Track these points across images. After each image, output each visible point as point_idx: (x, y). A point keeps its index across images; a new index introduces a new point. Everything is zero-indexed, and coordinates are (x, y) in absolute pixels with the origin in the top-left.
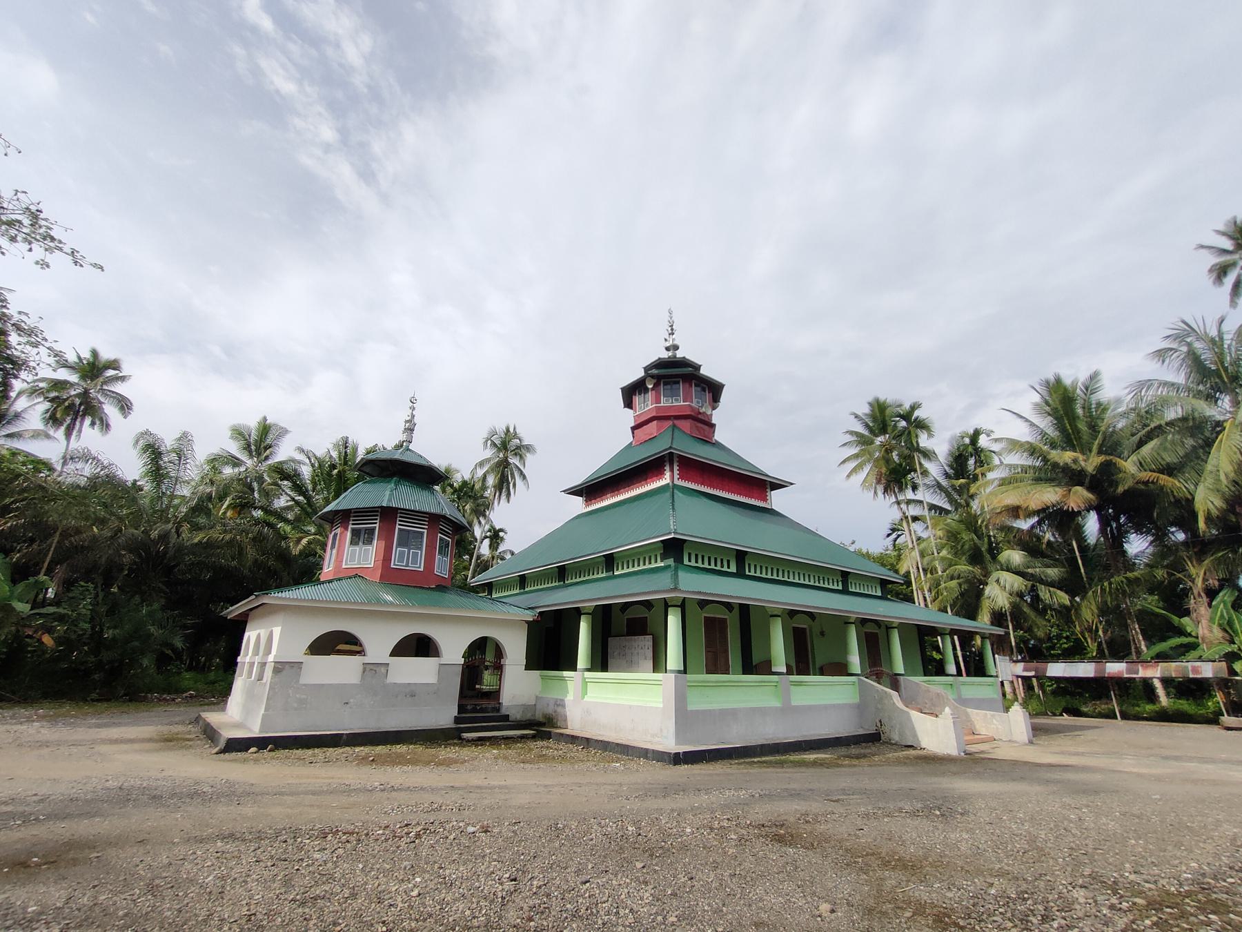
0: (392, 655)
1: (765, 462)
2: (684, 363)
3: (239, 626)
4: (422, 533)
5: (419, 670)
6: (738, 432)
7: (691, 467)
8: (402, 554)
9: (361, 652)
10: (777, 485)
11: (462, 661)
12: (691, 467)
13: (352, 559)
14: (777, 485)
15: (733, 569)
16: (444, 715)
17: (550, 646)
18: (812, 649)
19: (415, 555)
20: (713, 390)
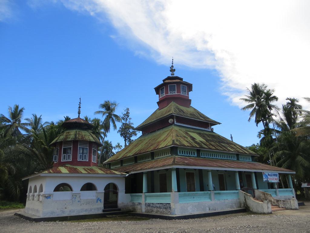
0: (54, 191)
1: (212, 116)
2: (177, 78)
3: (27, 182)
4: (87, 148)
5: (89, 195)
6: (200, 103)
7: (181, 120)
8: (65, 156)
9: (72, 190)
10: (215, 123)
11: (104, 191)
12: (181, 120)
13: (64, 158)
14: (215, 123)
15: (196, 155)
16: (98, 207)
17: (133, 185)
18: (224, 182)
19: (69, 156)
20: (189, 87)
